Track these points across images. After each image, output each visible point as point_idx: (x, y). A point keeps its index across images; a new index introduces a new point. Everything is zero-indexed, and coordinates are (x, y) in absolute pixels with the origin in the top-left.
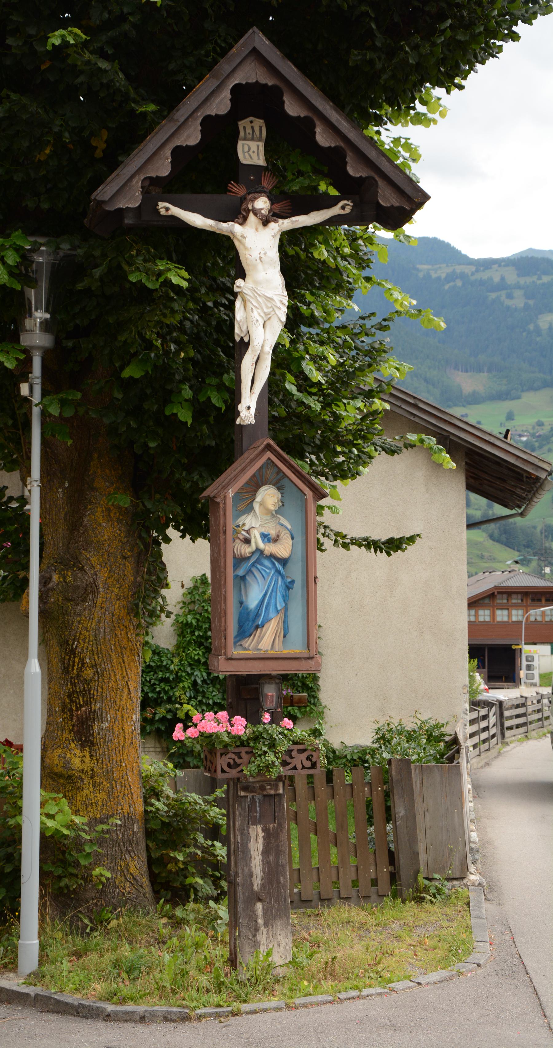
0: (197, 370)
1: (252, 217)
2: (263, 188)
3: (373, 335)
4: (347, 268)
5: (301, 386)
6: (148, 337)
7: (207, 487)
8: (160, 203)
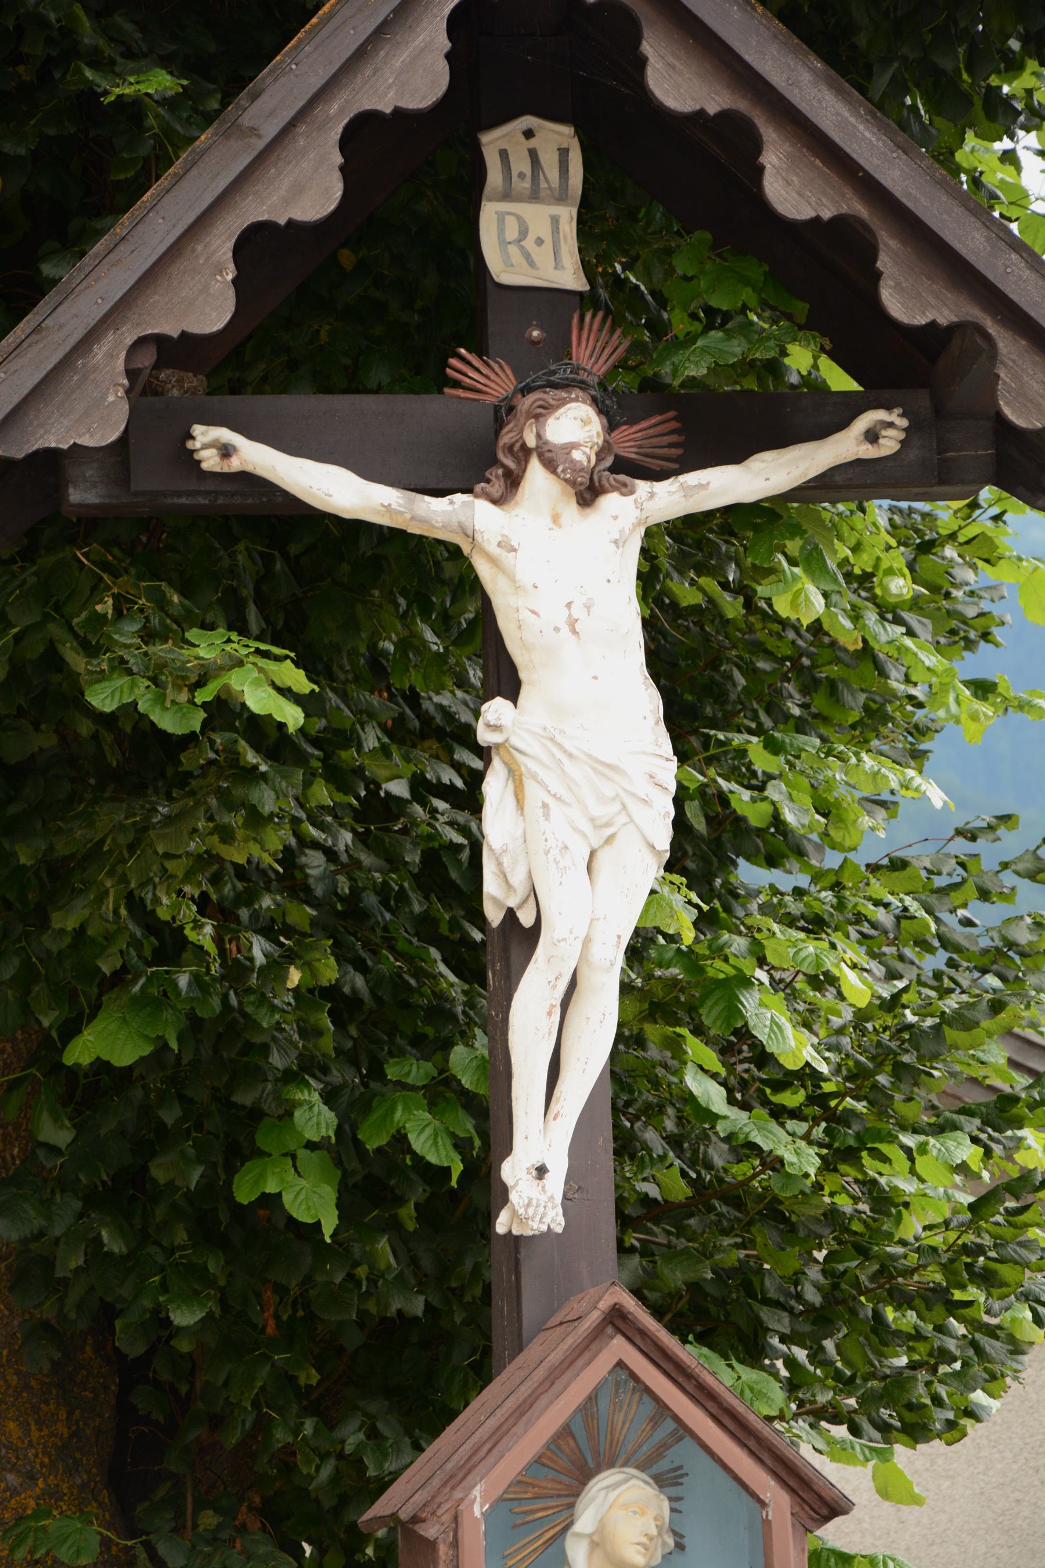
0: (354, 1032)
1: (536, 473)
2: (576, 370)
3: (1008, 896)
4: (902, 649)
5: (744, 1085)
6: (164, 914)
7: (395, 1475)
8: (198, 430)
